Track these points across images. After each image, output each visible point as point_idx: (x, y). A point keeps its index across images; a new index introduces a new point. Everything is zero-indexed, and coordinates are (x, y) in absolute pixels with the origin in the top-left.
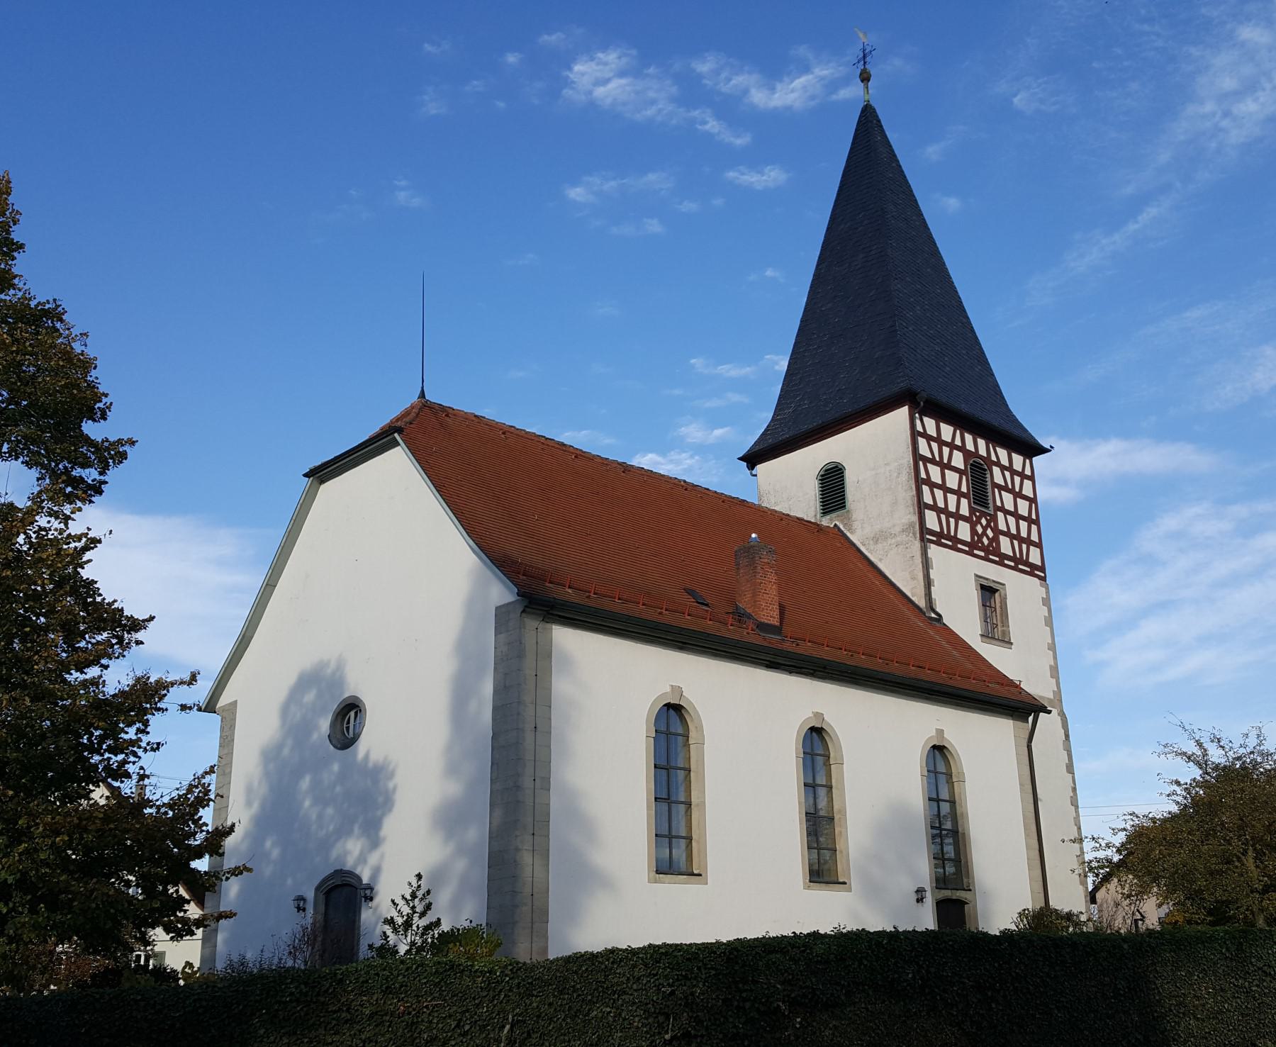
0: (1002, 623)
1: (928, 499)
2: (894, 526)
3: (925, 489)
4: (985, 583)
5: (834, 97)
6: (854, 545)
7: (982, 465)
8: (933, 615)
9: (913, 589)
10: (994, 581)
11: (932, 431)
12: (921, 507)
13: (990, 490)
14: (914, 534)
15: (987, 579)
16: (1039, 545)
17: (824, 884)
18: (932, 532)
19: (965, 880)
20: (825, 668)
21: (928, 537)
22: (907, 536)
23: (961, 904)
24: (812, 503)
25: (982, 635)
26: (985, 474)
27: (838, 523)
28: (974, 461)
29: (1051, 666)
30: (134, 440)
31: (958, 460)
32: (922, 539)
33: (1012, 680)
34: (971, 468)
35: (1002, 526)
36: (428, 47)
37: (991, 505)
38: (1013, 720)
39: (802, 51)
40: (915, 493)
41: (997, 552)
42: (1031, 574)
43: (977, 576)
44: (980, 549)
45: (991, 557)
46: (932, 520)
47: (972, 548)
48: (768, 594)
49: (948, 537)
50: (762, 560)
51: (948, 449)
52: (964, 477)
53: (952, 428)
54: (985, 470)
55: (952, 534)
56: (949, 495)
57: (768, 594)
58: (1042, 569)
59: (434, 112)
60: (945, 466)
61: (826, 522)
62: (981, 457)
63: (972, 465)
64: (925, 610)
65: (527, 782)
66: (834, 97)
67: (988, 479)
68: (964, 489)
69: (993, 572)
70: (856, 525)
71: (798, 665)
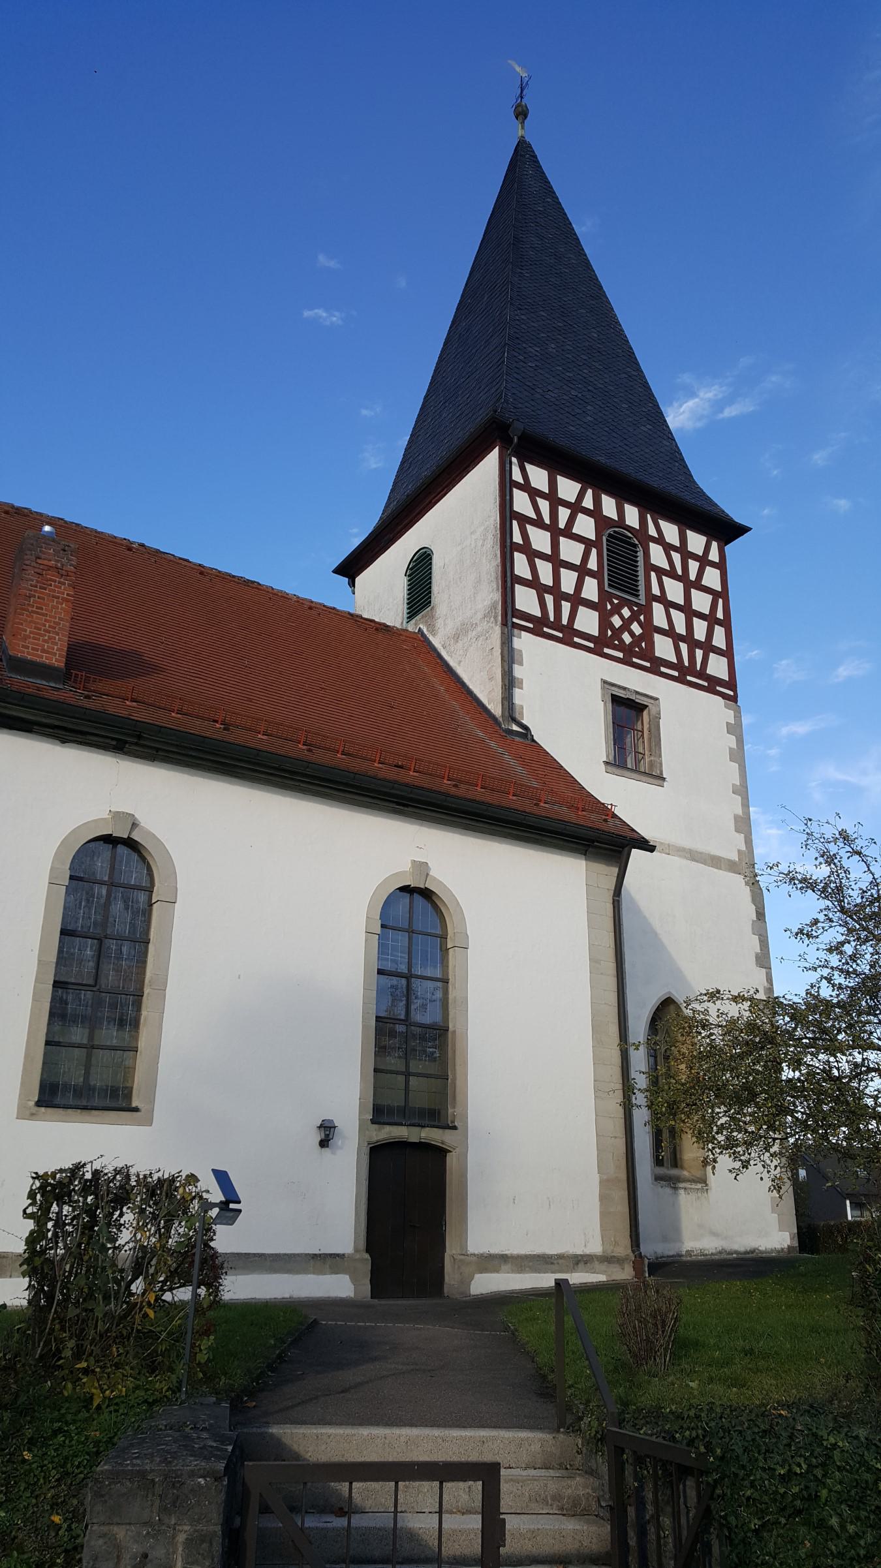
0: (650, 751)
2: (475, 613)
4: (621, 694)
5: (721, 416)
6: (435, 650)
7: (630, 538)
8: (515, 728)
9: (488, 693)
10: (637, 693)
12: (508, 580)
14: (495, 617)
15: (625, 689)
17: (79, 1111)
19: (450, 1111)
20: (139, 737)
21: (515, 620)
22: (488, 622)
23: (439, 1153)
24: (401, 607)
25: (606, 763)
26: (637, 557)
27: (422, 627)
28: (615, 532)
29: (736, 817)
32: (504, 624)
33: (603, 804)
34: (607, 540)
36: (364, 412)
37: (642, 593)
38: (586, 860)
39: (686, 378)
40: (499, 560)
41: (648, 654)
42: (711, 690)
43: (605, 682)
44: (615, 648)
45: (635, 660)
46: (526, 600)
47: (599, 645)
48: (43, 615)
50: (39, 561)
52: (594, 551)
53: (579, 486)
54: (635, 546)
55: (565, 621)
57: (43, 615)
58: (731, 684)
59: (374, 466)
61: (411, 627)
63: (610, 535)
64: (501, 720)
66: (721, 416)
67: (641, 559)
68: (593, 564)
70: (439, 623)
71: (70, 726)
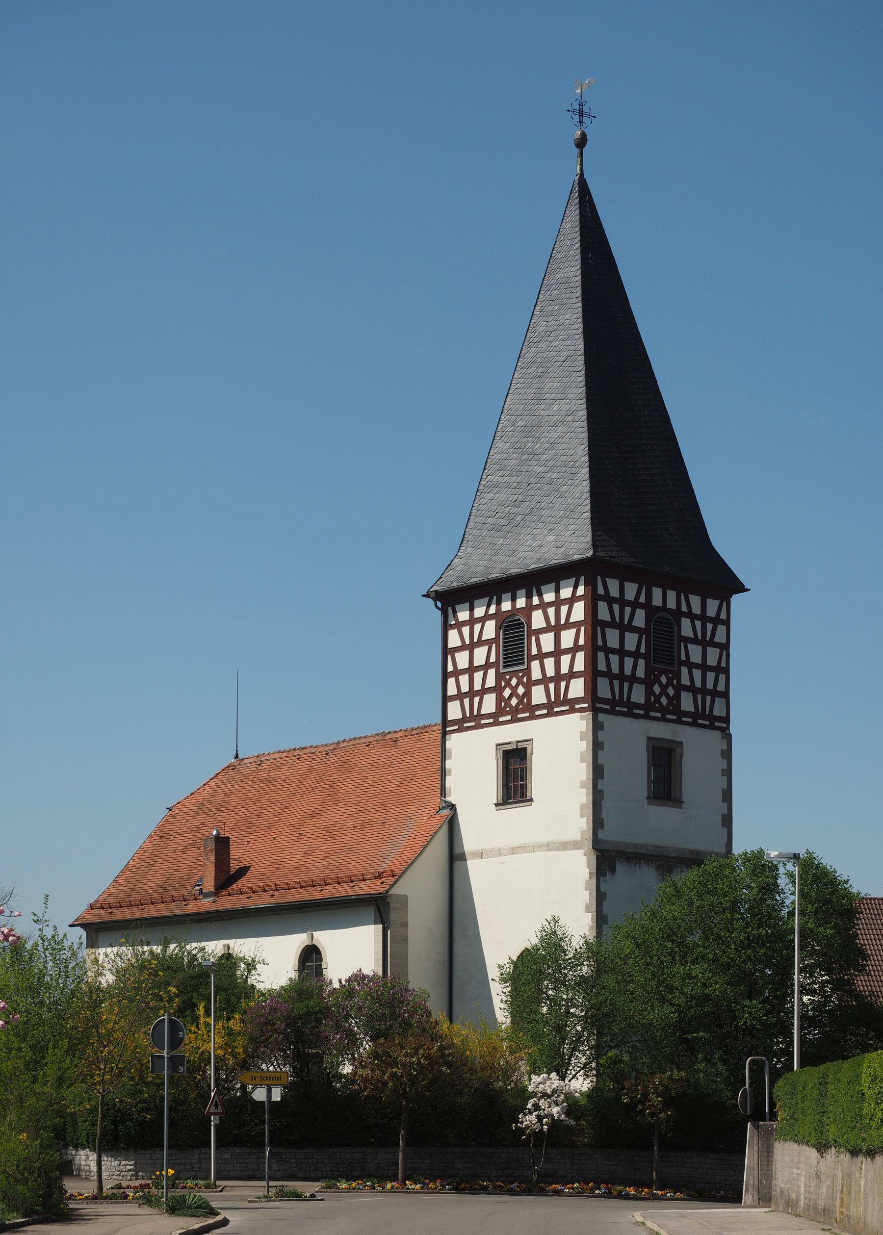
1: (602, 666)
3: (601, 656)
11: (614, 591)
18: (604, 701)
28: (659, 617)
29: (723, 815)
35: (685, 680)
42: (711, 727)
49: (621, 702)
60: (624, 628)
65: (644, 851)
69: (663, 731)
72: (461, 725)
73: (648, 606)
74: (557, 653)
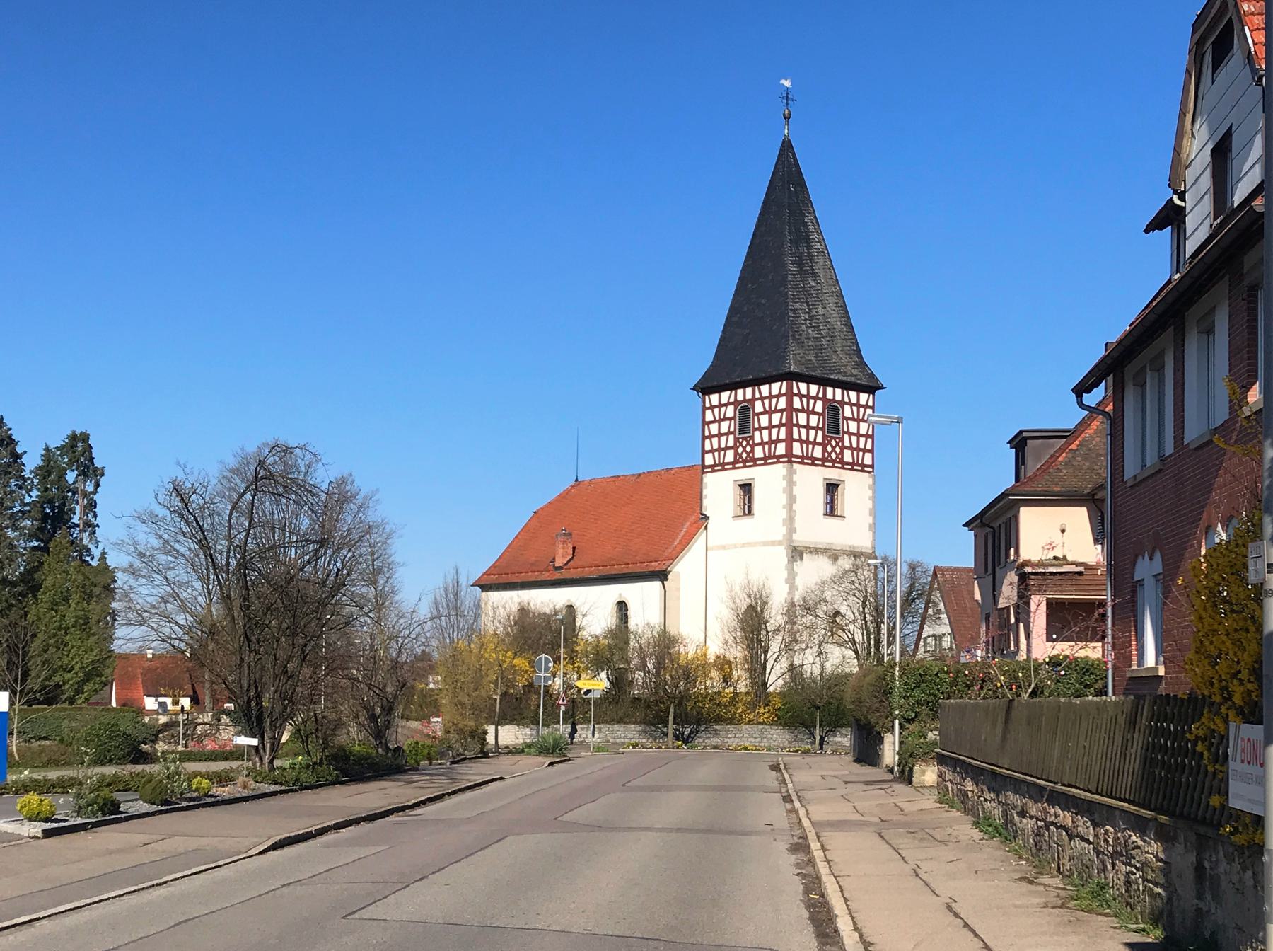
3: (795, 429)
4: (741, 483)
13: (840, 420)
16: (871, 451)
30: (967, 528)
31: (819, 407)
44: (749, 462)
51: (828, 397)
56: (801, 429)
60: (809, 412)
62: (837, 402)
72: (713, 468)
73: (824, 399)
74: (770, 427)
